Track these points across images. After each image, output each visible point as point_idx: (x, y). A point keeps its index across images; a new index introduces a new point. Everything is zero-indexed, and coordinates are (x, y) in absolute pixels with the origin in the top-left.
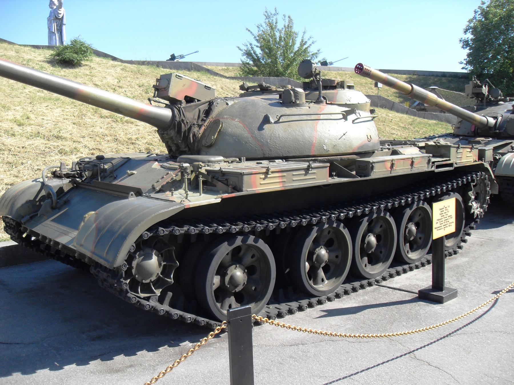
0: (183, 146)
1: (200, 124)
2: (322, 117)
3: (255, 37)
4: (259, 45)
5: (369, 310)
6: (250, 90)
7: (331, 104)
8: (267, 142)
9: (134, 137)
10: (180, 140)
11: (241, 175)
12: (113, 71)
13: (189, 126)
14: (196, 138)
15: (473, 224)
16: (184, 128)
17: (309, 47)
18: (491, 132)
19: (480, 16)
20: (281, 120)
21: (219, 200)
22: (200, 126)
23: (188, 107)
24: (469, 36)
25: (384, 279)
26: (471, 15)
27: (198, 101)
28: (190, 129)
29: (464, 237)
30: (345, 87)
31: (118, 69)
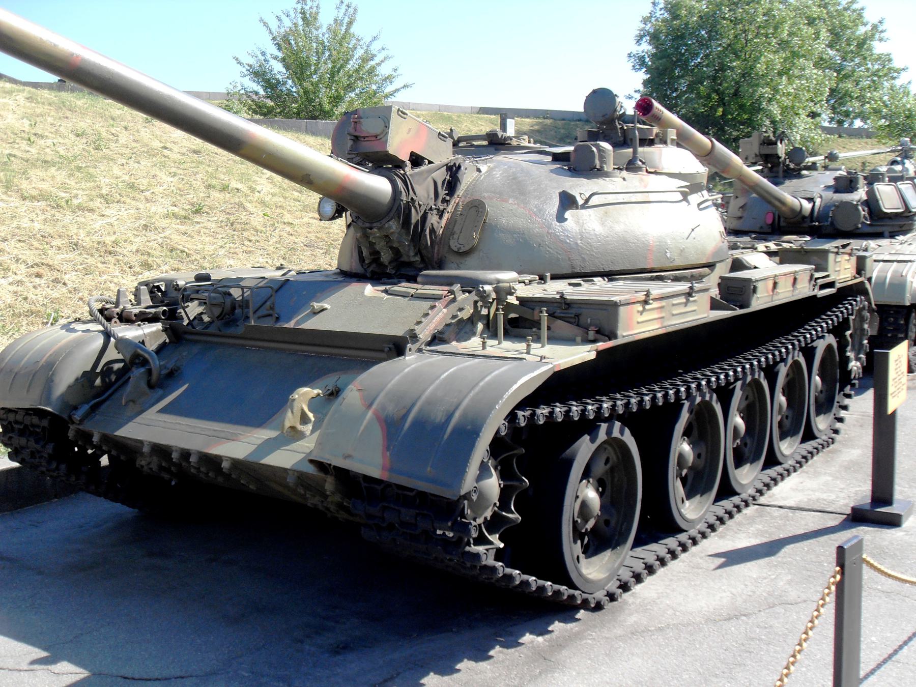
0: (412, 253)
1: (441, 208)
2: (652, 197)
3: (274, 39)
4: (280, 55)
5: (792, 546)
6: (461, 144)
7: (656, 173)
8: (577, 244)
9: (109, 239)
10: (407, 241)
11: (615, 305)
12: (11, 102)
13: (421, 214)
14: (436, 237)
15: (848, 390)
16: (415, 217)
17: (379, 64)
18: (805, 225)
19: (662, 12)
20: (591, 203)
21: (592, 356)
22: (441, 214)
23: (417, 174)
24: (646, 47)
25: (760, 492)
26: (647, 9)
27: (430, 162)
28: (424, 217)
29: (839, 413)
30: (669, 141)
31: (21, 98)
